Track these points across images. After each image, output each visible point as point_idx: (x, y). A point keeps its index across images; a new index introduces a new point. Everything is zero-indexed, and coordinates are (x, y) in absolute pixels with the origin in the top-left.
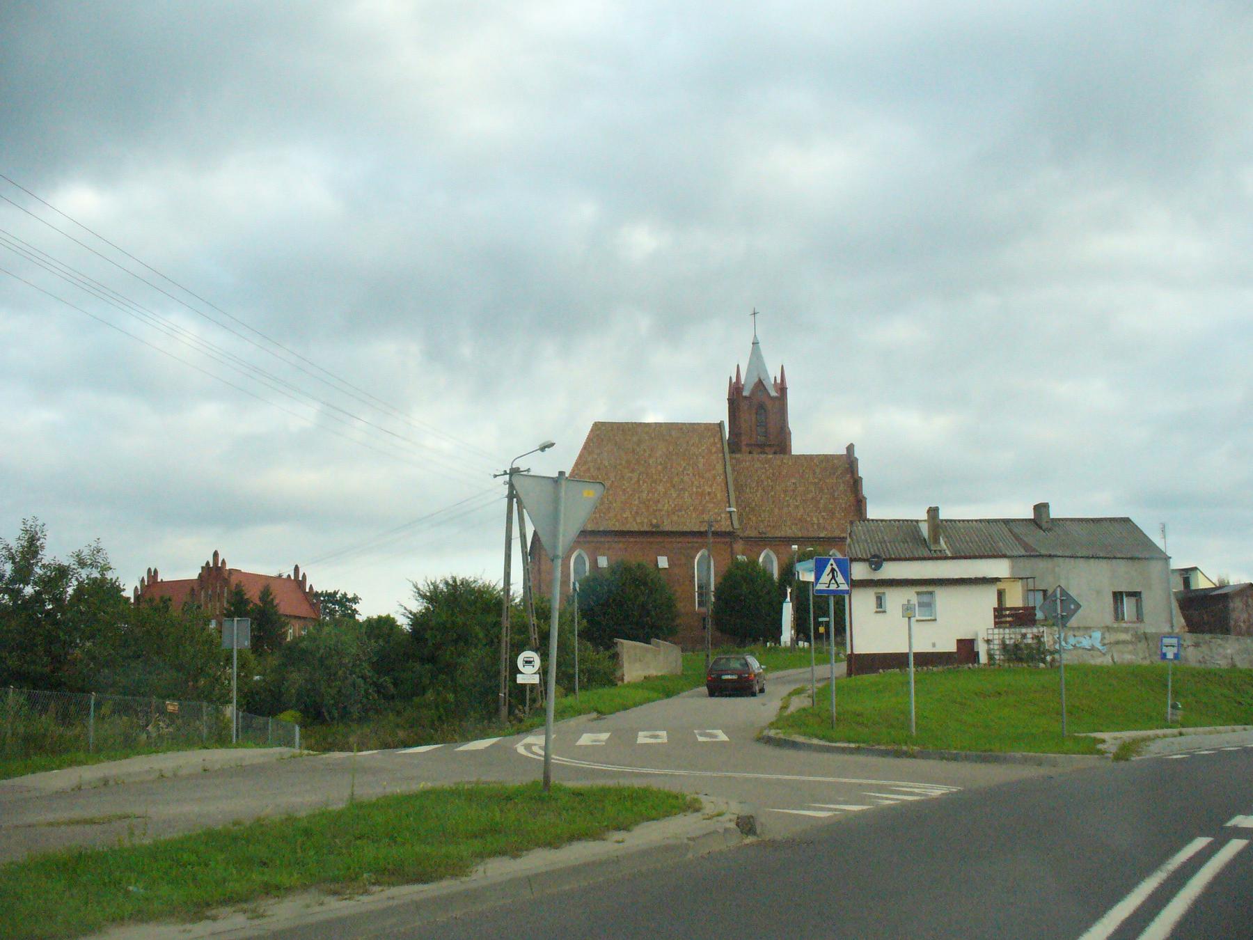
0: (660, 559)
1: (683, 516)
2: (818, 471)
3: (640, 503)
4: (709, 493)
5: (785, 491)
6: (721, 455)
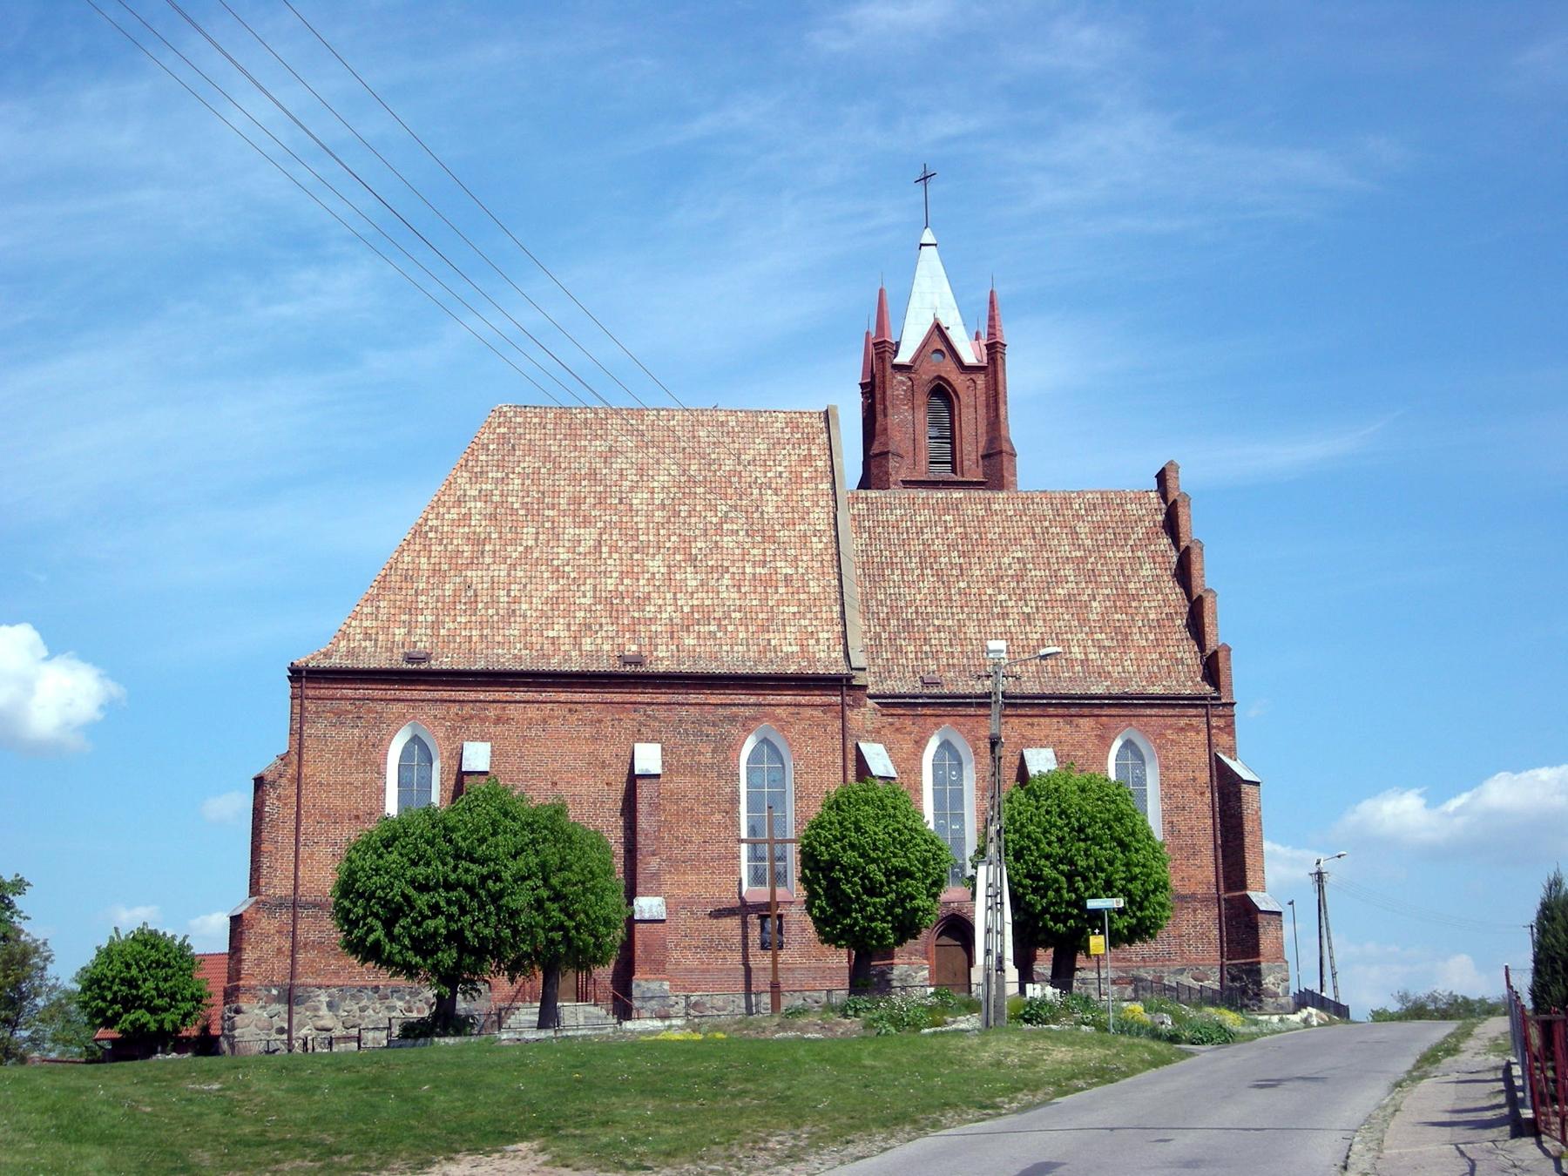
0: (641, 749)
1: (712, 634)
2: (1083, 529)
3: (597, 599)
4: (788, 580)
5: (995, 582)
6: (826, 486)
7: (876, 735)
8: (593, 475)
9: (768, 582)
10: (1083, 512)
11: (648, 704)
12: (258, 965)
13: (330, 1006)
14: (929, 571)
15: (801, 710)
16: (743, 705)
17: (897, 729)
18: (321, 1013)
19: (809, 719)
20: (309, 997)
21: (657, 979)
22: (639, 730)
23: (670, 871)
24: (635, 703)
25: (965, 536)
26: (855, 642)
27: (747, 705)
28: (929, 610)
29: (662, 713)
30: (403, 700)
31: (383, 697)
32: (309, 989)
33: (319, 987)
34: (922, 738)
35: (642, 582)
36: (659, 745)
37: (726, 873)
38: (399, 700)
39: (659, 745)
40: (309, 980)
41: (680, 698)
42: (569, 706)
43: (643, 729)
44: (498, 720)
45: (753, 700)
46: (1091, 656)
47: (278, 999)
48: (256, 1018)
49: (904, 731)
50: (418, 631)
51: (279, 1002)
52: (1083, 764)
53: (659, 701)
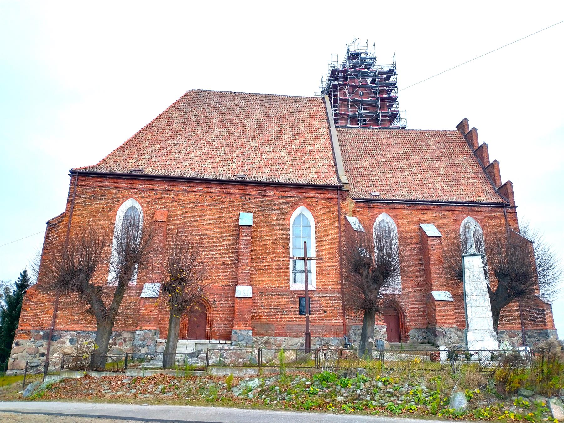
7: (354, 213)
8: (228, 113)
9: (302, 151)
10: (430, 137)
12: (34, 319)
13: (71, 341)
14: (368, 155)
15: (319, 201)
16: (292, 197)
17: (361, 214)
18: (65, 345)
19: (322, 205)
20: (60, 336)
21: (245, 329)
22: (242, 207)
23: (255, 274)
25: (382, 144)
26: (341, 172)
27: (294, 197)
28: (370, 168)
29: (254, 199)
30: (127, 188)
31: (117, 186)
32: (60, 332)
33: (67, 331)
35: (247, 149)
36: (252, 214)
37: (282, 276)
38: (125, 188)
39: (252, 214)
40: (61, 327)
41: (262, 193)
42: (209, 194)
43: (244, 206)
44: (174, 200)
45: (296, 195)
46: (444, 188)
47: (43, 337)
48: (28, 347)
50: (141, 162)
51: (43, 339)
52: (448, 232)
53: (252, 193)
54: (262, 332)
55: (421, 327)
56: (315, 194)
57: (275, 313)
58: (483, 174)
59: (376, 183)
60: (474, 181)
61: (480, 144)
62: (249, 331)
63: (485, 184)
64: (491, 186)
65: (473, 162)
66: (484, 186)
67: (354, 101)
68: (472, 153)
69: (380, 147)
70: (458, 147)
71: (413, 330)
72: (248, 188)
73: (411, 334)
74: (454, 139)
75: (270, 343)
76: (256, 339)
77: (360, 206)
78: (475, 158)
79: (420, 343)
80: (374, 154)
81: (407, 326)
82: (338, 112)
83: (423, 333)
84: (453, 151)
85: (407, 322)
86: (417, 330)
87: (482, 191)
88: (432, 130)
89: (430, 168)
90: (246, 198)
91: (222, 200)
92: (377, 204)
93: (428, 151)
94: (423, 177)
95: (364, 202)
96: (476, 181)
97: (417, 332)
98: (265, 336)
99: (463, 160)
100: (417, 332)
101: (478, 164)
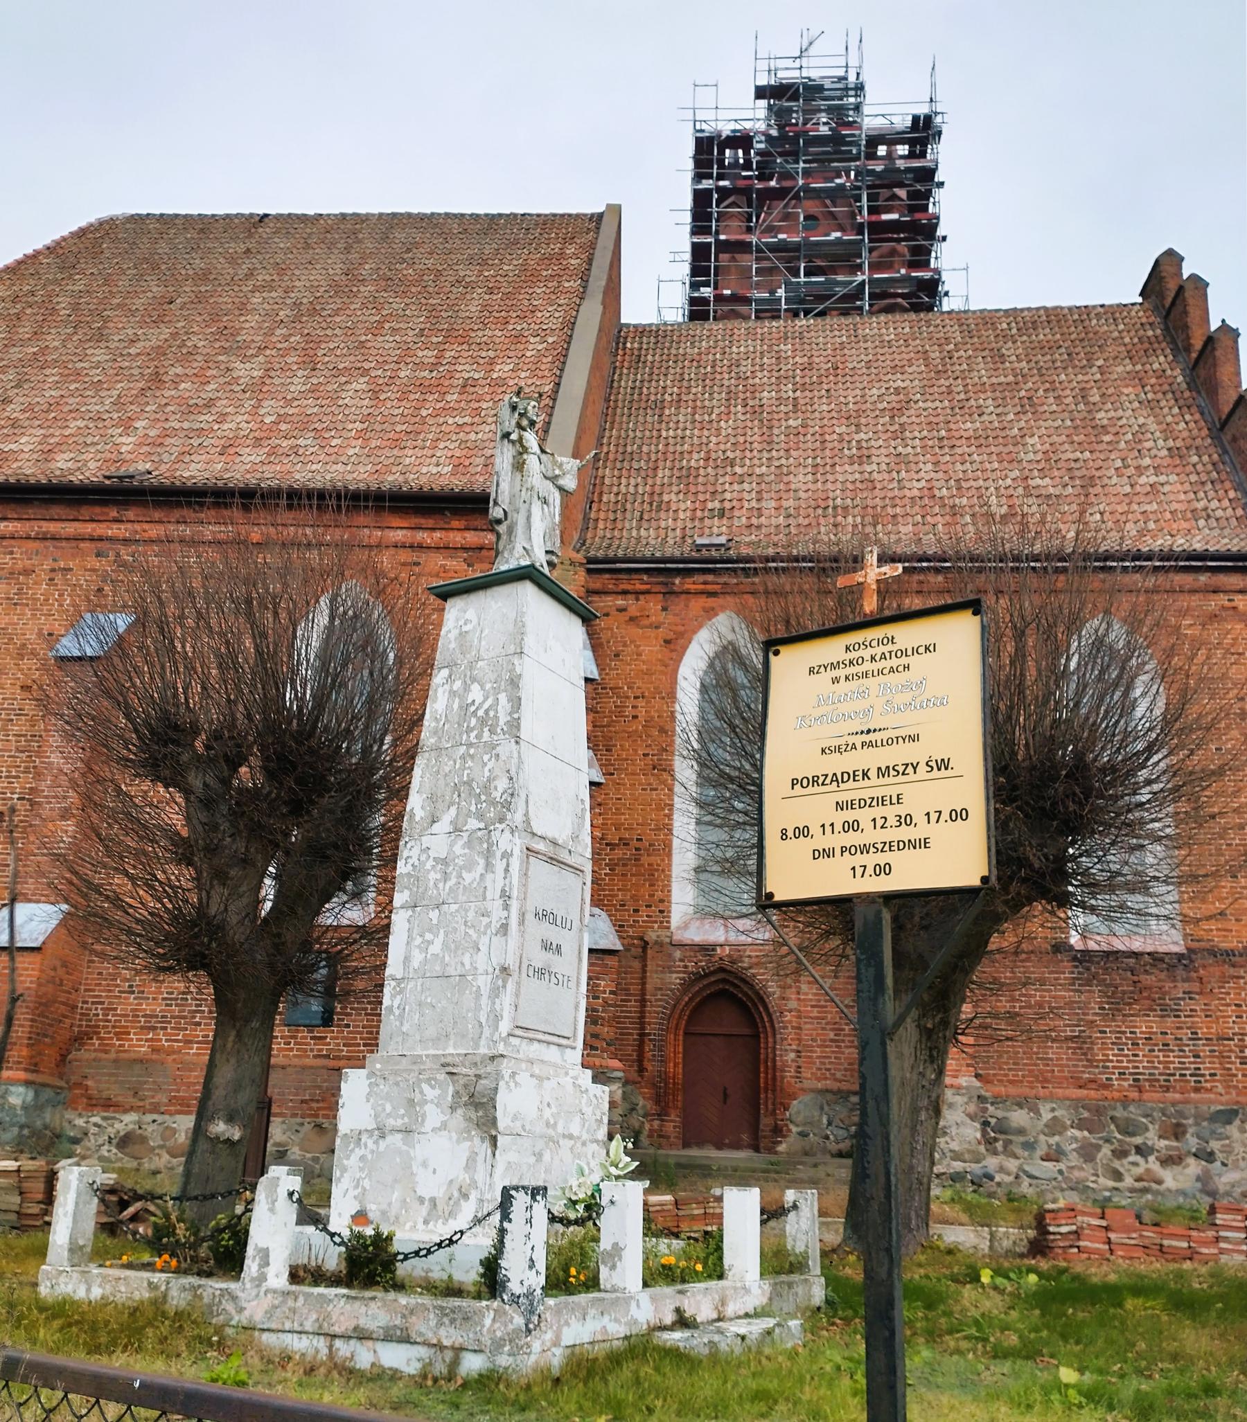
11: (126, 541)
15: (423, 557)
17: (632, 619)
24: (100, 539)
25: (810, 366)
34: (680, 635)
49: (646, 622)
54: (113, 1091)
55: (845, 1086)
56: (409, 533)
57: (184, 1017)
58: (1212, 450)
59: (735, 503)
60: (1162, 479)
61: (1214, 325)
62: (13, 1089)
63: (1209, 486)
64: (1232, 494)
65: (1176, 410)
66: (1201, 494)
67: (774, 248)
68: (1180, 379)
69: (798, 379)
70: (1127, 361)
71: (807, 1098)
72: (130, 514)
73: (798, 1112)
74: (1116, 334)
75: (143, 1140)
76: (87, 1122)
77: (629, 587)
78: (1187, 394)
79: (833, 1156)
80: (764, 401)
81: (783, 1078)
82: (707, 292)
83: (852, 1110)
84: (1098, 376)
85: (785, 1065)
86: (829, 1096)
87: (1189, 515)
88: (1029, 309)
89: (979, 441)
90: (118, 555)
91: (20, 565)
92: (700, 578)
93: (994, 380)
94: (941, 475)
95: (646, 571)
96: (1173, 478)
97: (826, 1108)
98: (126, 1111)
99: (1136, 404)
100: (826, 1108)
101: (1197, 416)
